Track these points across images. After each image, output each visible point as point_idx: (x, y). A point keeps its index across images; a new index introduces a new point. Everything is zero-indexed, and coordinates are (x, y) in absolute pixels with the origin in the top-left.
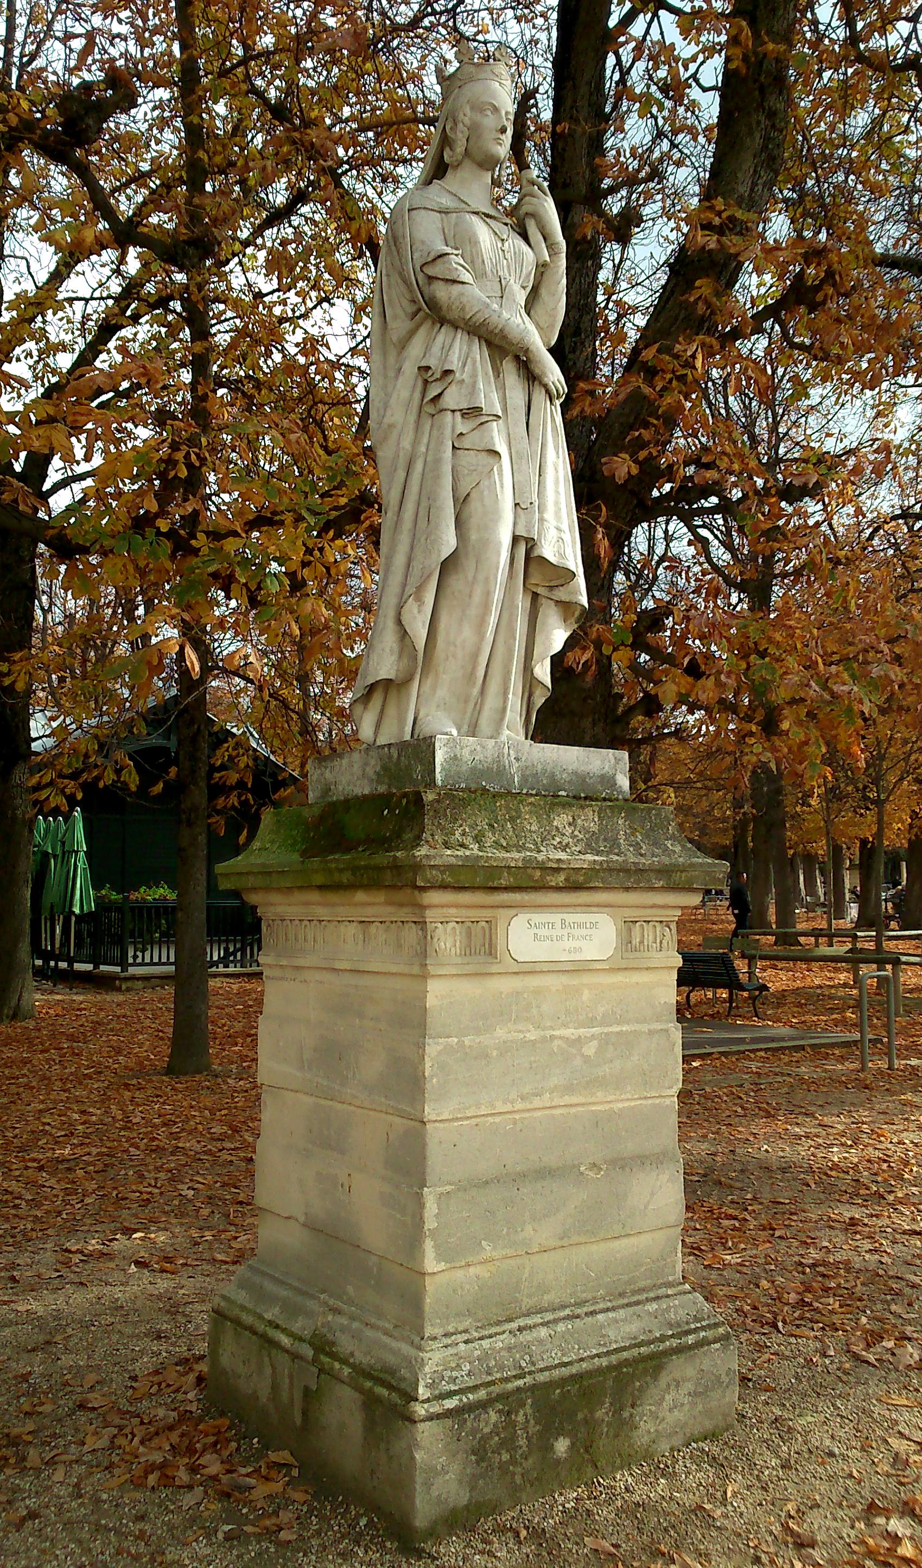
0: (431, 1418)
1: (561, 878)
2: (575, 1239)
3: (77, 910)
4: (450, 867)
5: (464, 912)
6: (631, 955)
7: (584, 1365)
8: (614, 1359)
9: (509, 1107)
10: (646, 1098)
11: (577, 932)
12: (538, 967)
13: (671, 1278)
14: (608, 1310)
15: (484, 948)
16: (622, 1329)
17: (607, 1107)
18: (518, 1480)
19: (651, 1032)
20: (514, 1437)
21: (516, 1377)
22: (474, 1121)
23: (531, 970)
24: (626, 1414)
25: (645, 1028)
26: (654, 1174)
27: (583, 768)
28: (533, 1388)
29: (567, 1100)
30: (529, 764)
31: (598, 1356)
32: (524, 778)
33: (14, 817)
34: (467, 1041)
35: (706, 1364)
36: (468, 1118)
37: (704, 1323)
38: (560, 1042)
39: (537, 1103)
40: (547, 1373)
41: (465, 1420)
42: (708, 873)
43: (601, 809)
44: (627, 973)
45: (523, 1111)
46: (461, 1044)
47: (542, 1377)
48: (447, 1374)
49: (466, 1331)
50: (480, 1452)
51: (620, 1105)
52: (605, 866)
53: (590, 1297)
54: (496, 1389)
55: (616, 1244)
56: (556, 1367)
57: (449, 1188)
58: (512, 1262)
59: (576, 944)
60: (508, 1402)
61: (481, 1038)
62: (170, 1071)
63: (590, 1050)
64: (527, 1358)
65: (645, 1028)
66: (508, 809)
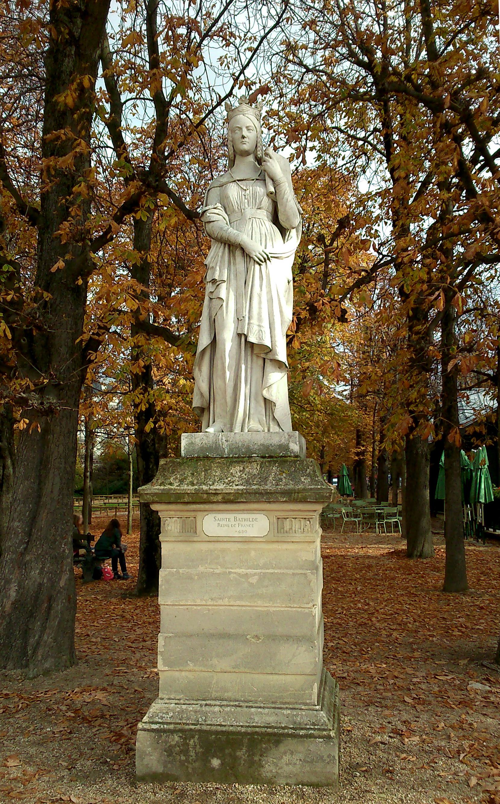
0: (144, 730)
1: (220, 498)
2: (242, 669)
3: (482, 500)
4: (156, 494)
5: (178, 513)
6: (280, 535)
7: (231, 728)
8: (249, 730)
9: (204, 603)
10: (290, 607)
11: (243, 523)
12: (220, 539)
13: (308, 701)
14: (260, 707)
15: (191, 531)
16: (263, 718)
17: (266, 609)
18: (190, 770)
19: (293, 574)
20: (187, 751)
21: (192, 724)
22: (186, 607)
23: (217, 540)
24: (256, 758)
25: (291, 572)
26: (295, 646)
27: (269, 442)
28: (200, 731)
29: (238, 603)
30: (234, 442)
31: (242, 726)
32: (231, 450)
33: (417, 453)
34: (181, 571)
35: (312, 747)
36: (181, 605)
37: (316, 727)
38: (235, 575)
39: (220, 602)
40: (209, 727)
41: (161, 736)
42: (318, 494)
43: (262, 463)
44: (280, 544)
45: (213, 605)
46: (178, 572)
47: (204, 728)
48: (160, 714)
49: (179, 700)
50: (169, 751)
51: (274, 609)
52: (245, 491)
53: (253, 699)
54: (179, 727)
55: (271, 677)
56: (217, 725)
57: (171, 635)
58: (206, 674)
59: (244, 529)
60: (187, 734)
61: (189, 570)
62: (445, 589)
63: (254, 580)
64: (204, 718)
65: (291, 572)
66: (204, 466)
